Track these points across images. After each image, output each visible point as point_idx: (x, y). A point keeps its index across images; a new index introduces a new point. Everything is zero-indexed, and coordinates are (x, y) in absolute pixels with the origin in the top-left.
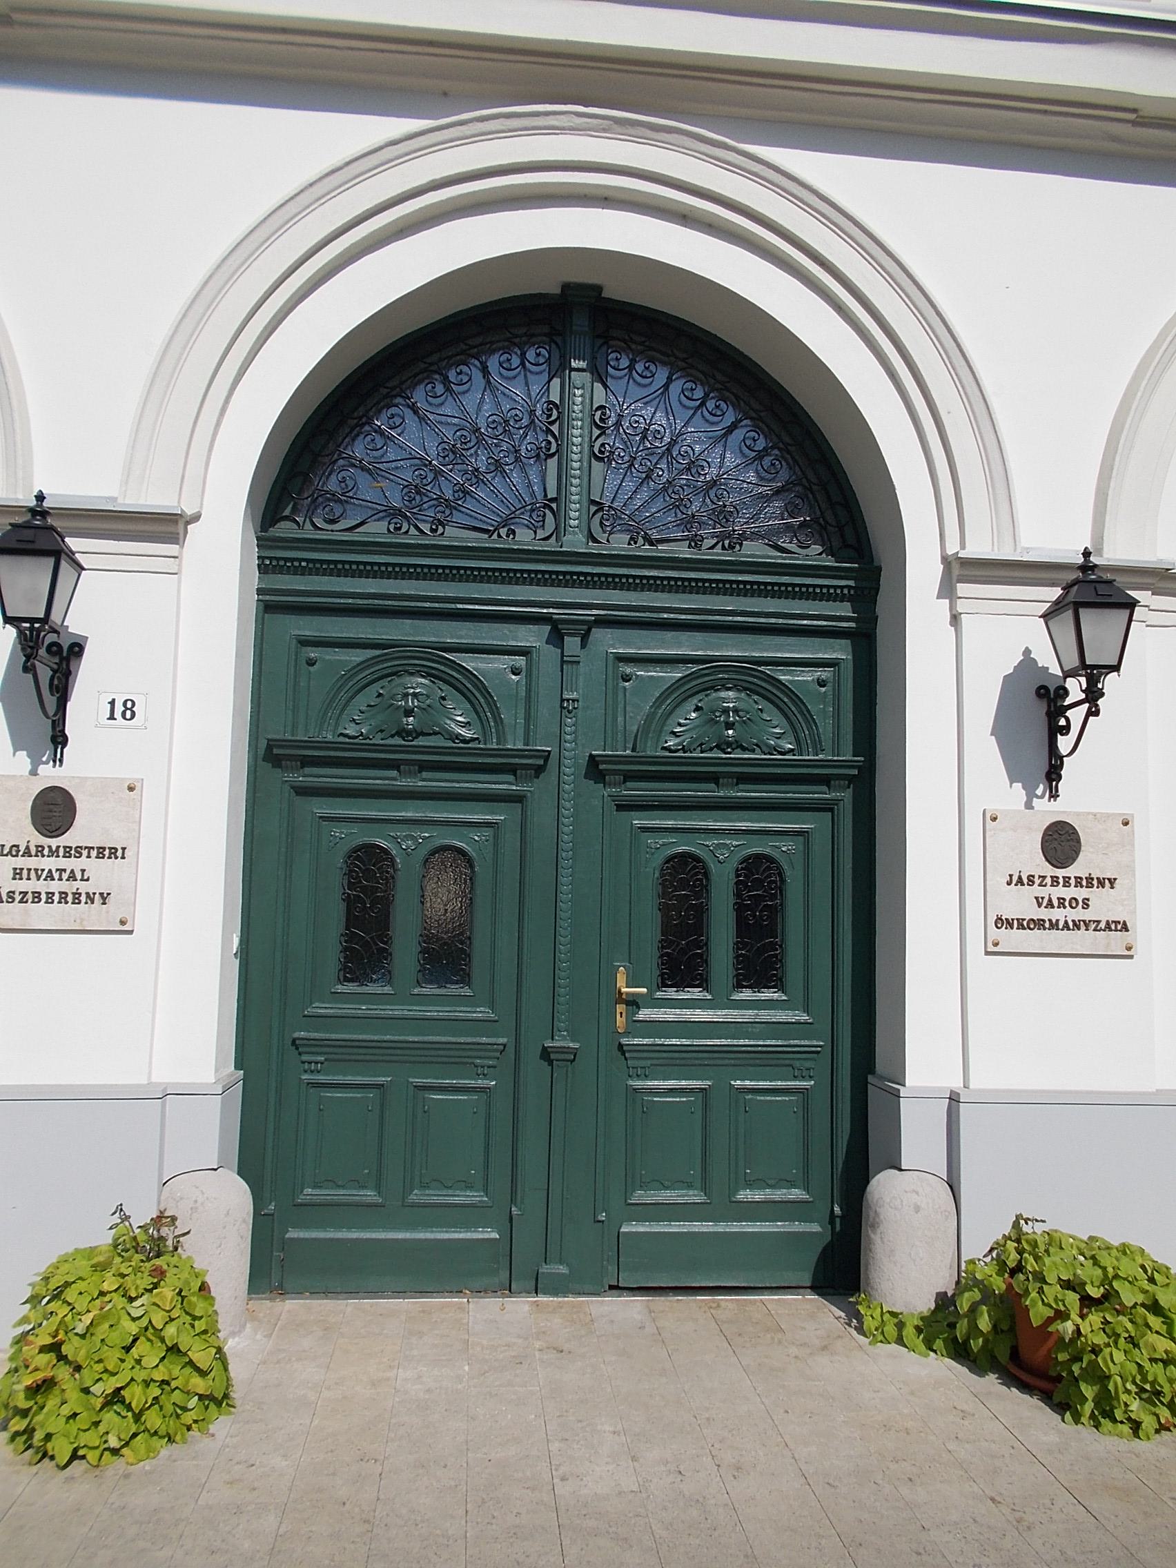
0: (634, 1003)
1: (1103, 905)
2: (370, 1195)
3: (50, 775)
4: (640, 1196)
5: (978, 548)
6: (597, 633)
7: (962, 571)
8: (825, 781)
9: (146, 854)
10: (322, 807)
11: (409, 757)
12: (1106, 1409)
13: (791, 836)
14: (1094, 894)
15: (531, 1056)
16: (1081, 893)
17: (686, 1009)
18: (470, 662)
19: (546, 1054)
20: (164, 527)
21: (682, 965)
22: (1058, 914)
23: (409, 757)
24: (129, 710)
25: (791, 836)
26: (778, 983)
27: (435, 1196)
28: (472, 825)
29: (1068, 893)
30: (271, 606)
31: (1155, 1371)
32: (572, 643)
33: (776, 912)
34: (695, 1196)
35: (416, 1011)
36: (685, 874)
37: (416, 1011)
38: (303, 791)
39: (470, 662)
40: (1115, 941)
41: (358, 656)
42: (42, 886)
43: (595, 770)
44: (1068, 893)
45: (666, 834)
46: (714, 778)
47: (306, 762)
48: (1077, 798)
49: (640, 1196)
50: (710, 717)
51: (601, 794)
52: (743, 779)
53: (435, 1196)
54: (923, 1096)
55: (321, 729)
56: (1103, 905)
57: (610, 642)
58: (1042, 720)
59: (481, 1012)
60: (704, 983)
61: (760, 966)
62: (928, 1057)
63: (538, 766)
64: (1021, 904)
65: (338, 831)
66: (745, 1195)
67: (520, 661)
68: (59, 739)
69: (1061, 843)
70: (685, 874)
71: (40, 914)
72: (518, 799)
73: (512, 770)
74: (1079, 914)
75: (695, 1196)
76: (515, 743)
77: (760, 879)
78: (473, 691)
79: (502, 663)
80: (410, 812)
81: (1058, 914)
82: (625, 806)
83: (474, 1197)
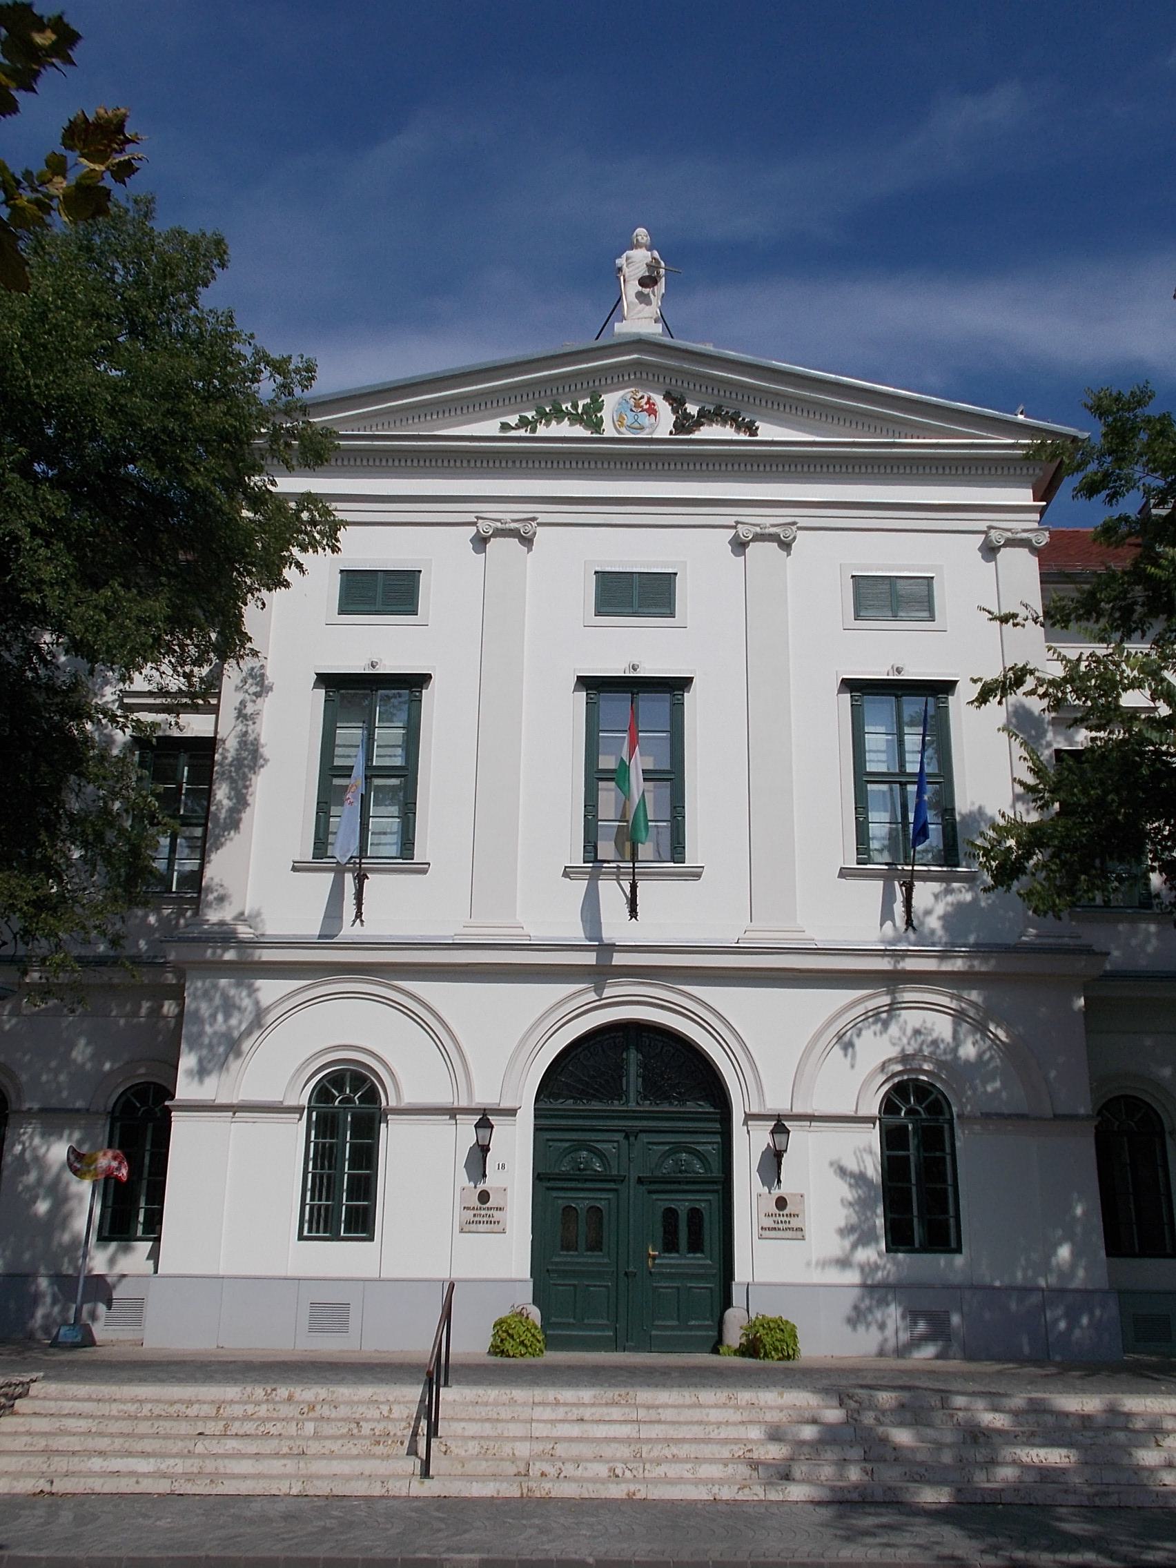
0: (654, 1258)
1: (795, 1223)
2: (572, 1321)
3: (481, 1186)
4: (657, 1323)
5: (755, 1110)
6: (641, 1136)
7: (749, 1117)
8: (715, 1183)
9: (508, 1209)
10: (555, 1194)
11: (581, 1178)
12: (766, 1355)
13: (706, 1202)
14: (792, 1220)
15: (621, 1274)
16: (788, 1219)
17: (672, 1259)
18: (598, 1146)
19: (626, 1274)
20: (512, 1112)
21: (670, 1245)
22: (780, 1226)
23: (581, 1178)
24: (503, 1166)
25: (706, 1202)
26: (702, 1251)
27: (592, 1321)
28: (602, 1200)
29: (784, 1219)
30: (537, 1129)
31: (777, 1344)
32: (632, 1139)
33: (701, 1226)
34: (675, 1323)
35: (585, 1260)
36: (670, 1215)
37: (585, 1260)
38: (548, 1189)
39: (598, 1146)
40: (799, 1234)
41: (567, 1145)
42: (481, 1219)
43: (640, 1181)
44: (784, 1219)
45: (663, 1202)
46: (679, 1183)
47: (549, 1180)
48: (787, 1187)
49: (657, 1323)
50: (676, 1162)
51: (643, 1188)
52: (688, 1183)
53: (592, 1321)
54: (740, 1284)
55: (185, 838)
56: (795, 1223)
57: (644, 1138)
58: (773, 1162)
59: (606, 1260)
60: (677, 1251)
61: (696, 1245)
62: (741, 1274)
63: (622, 1180)
64: (769, 1223)
65: (560, 1202)
66: (693, 1323)
67: (615, 1145)
68: (484, 1175)
69: (781, 1203)
70: (670, 1215)
71: (481, 1227)
72: (616, 1190)
73: (614, 1181)
74: (787, 1225)
75: (675, 1323)
76: (615, 1172)
77: (695, 1216)
78: (601, 1155)
79: (610, 1146)
80: (581, 1195)
81: (780, 1226)
82: (650, 1192)
83: (605, 1322)
